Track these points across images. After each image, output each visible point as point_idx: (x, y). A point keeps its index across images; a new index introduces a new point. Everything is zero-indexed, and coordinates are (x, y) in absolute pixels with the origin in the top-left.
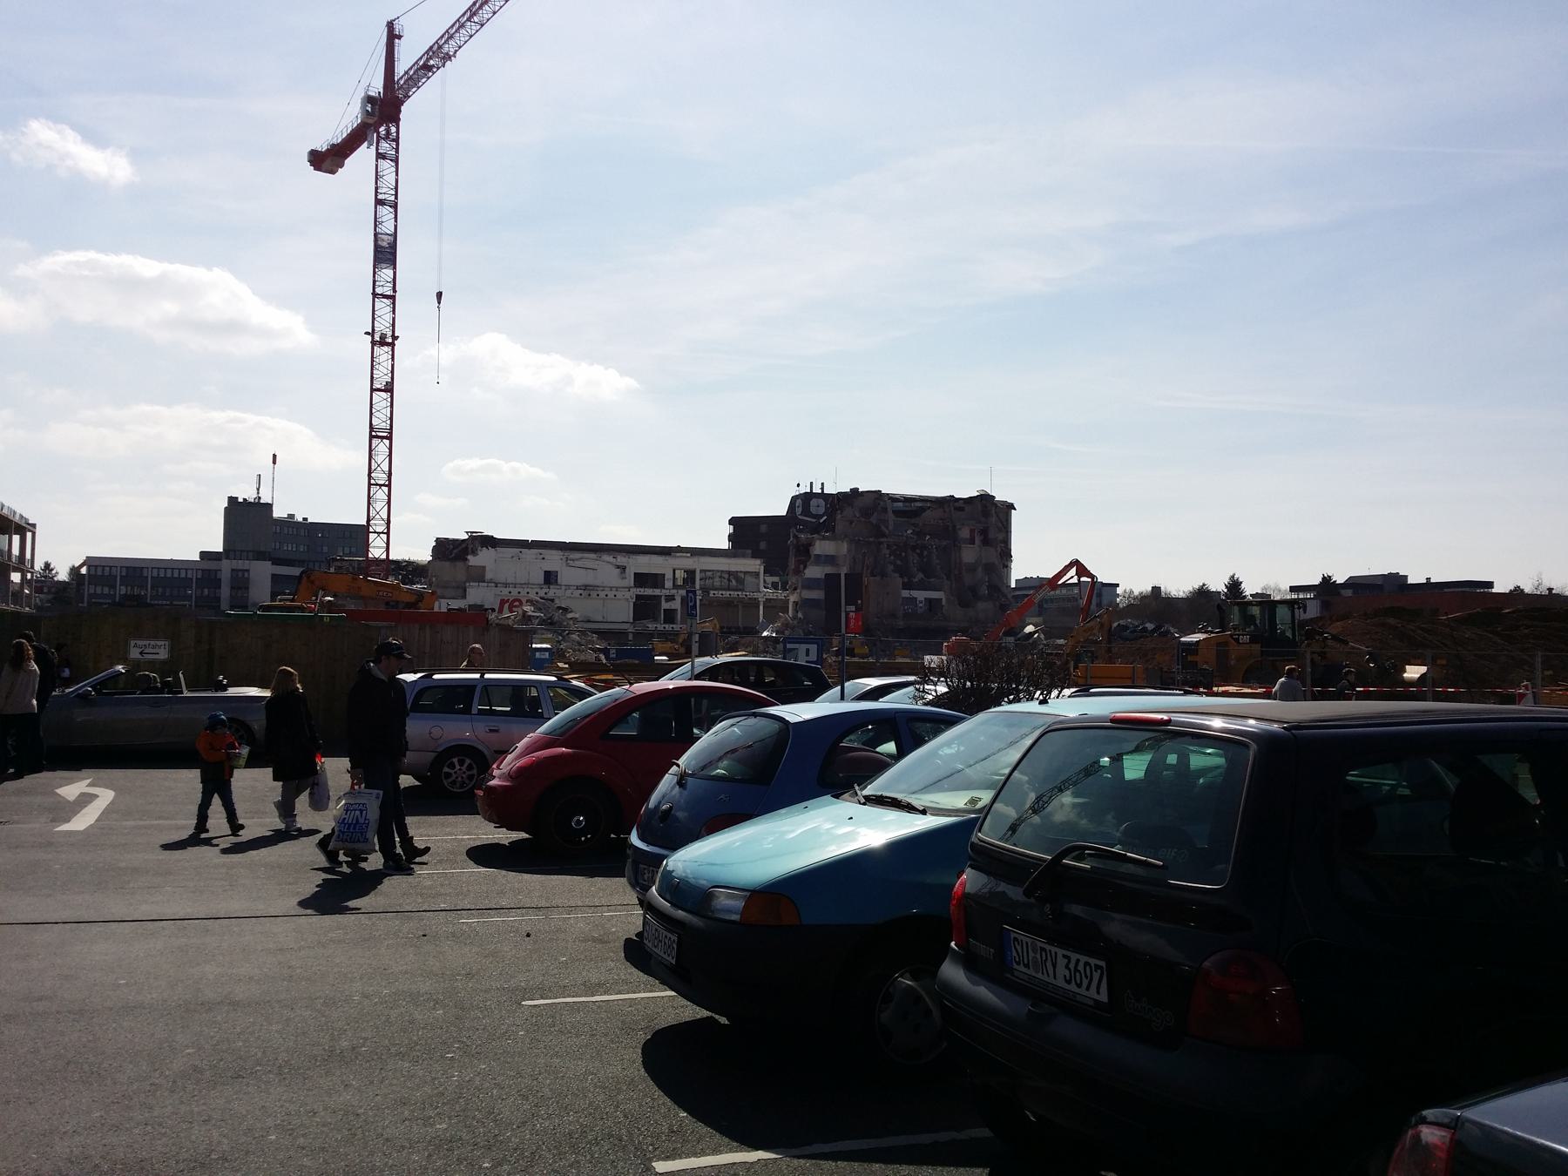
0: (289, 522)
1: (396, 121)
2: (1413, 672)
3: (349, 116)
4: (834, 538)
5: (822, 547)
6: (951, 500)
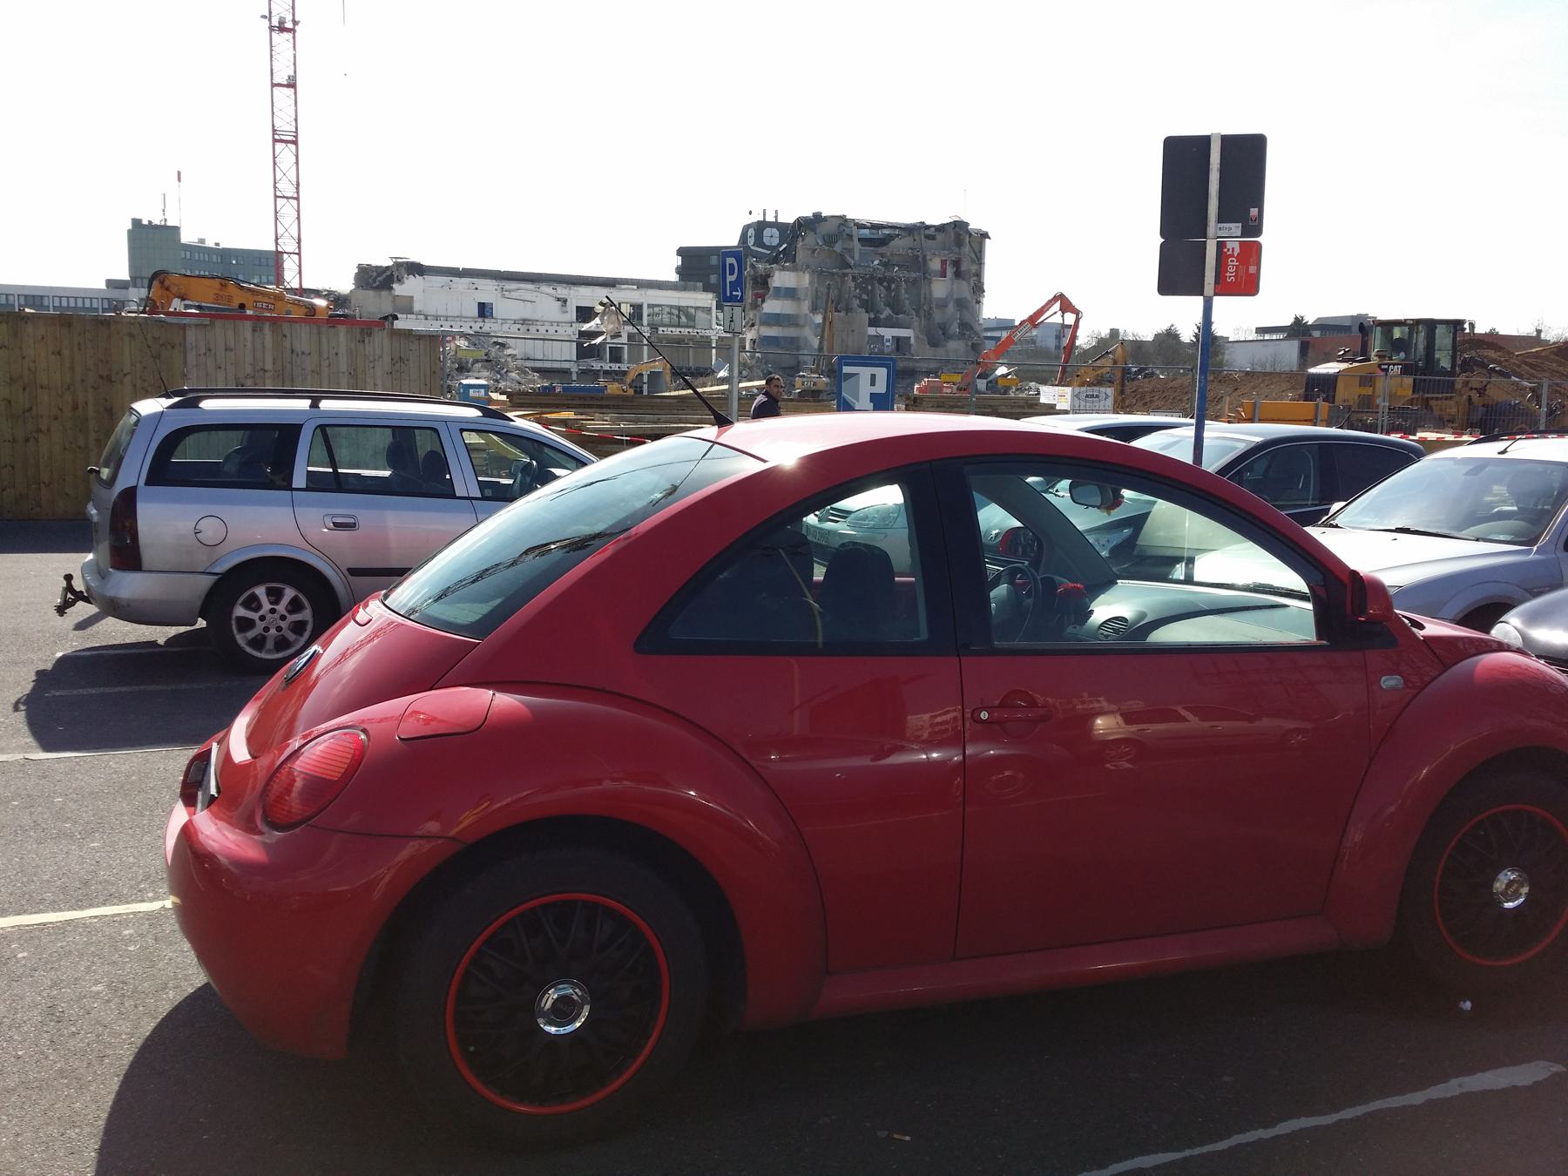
0: (199, 250)
4: (795, 269)
5: (782, 278)
6: (922, 227)
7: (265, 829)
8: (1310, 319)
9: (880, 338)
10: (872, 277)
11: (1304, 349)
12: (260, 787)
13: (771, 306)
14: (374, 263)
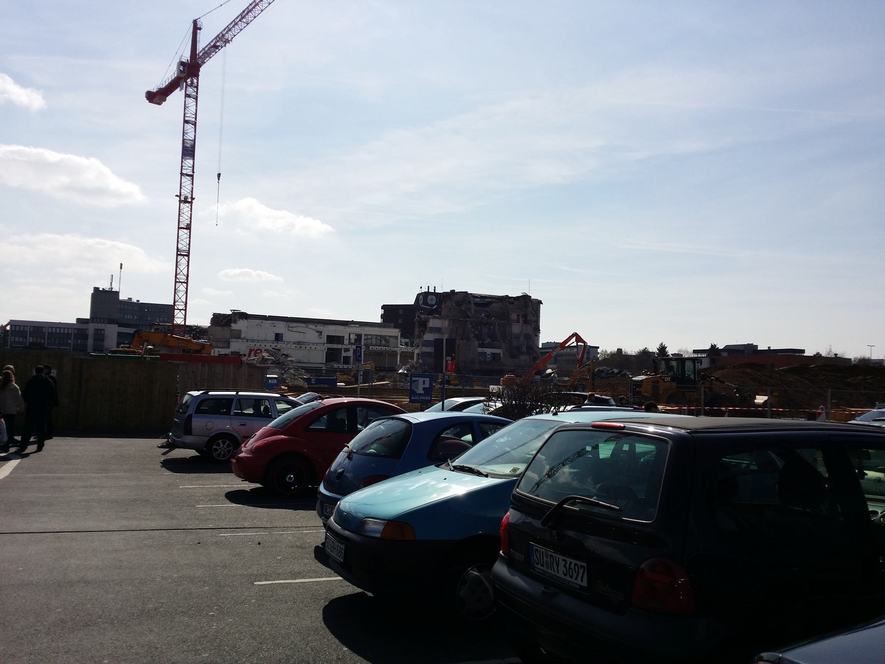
1: (197, 76)
3: (170, 72)
4: (440, 318)
5: (433, 323)
6: (507, 297)
8: (721, 346)
14: (222, 313)
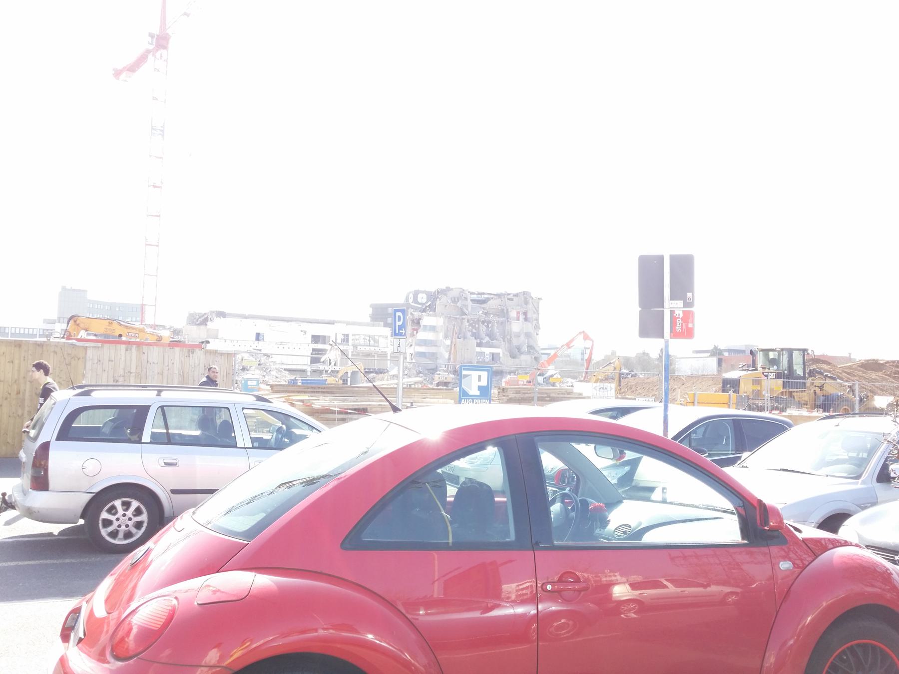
2: (881, 401)
4: (436, 316)
5: (428, 320)
7: (112, 660)
9: (482, 353)
10: (478, 320)
11: (720, 362)
12: (111, 632)
13: (422, 335)
